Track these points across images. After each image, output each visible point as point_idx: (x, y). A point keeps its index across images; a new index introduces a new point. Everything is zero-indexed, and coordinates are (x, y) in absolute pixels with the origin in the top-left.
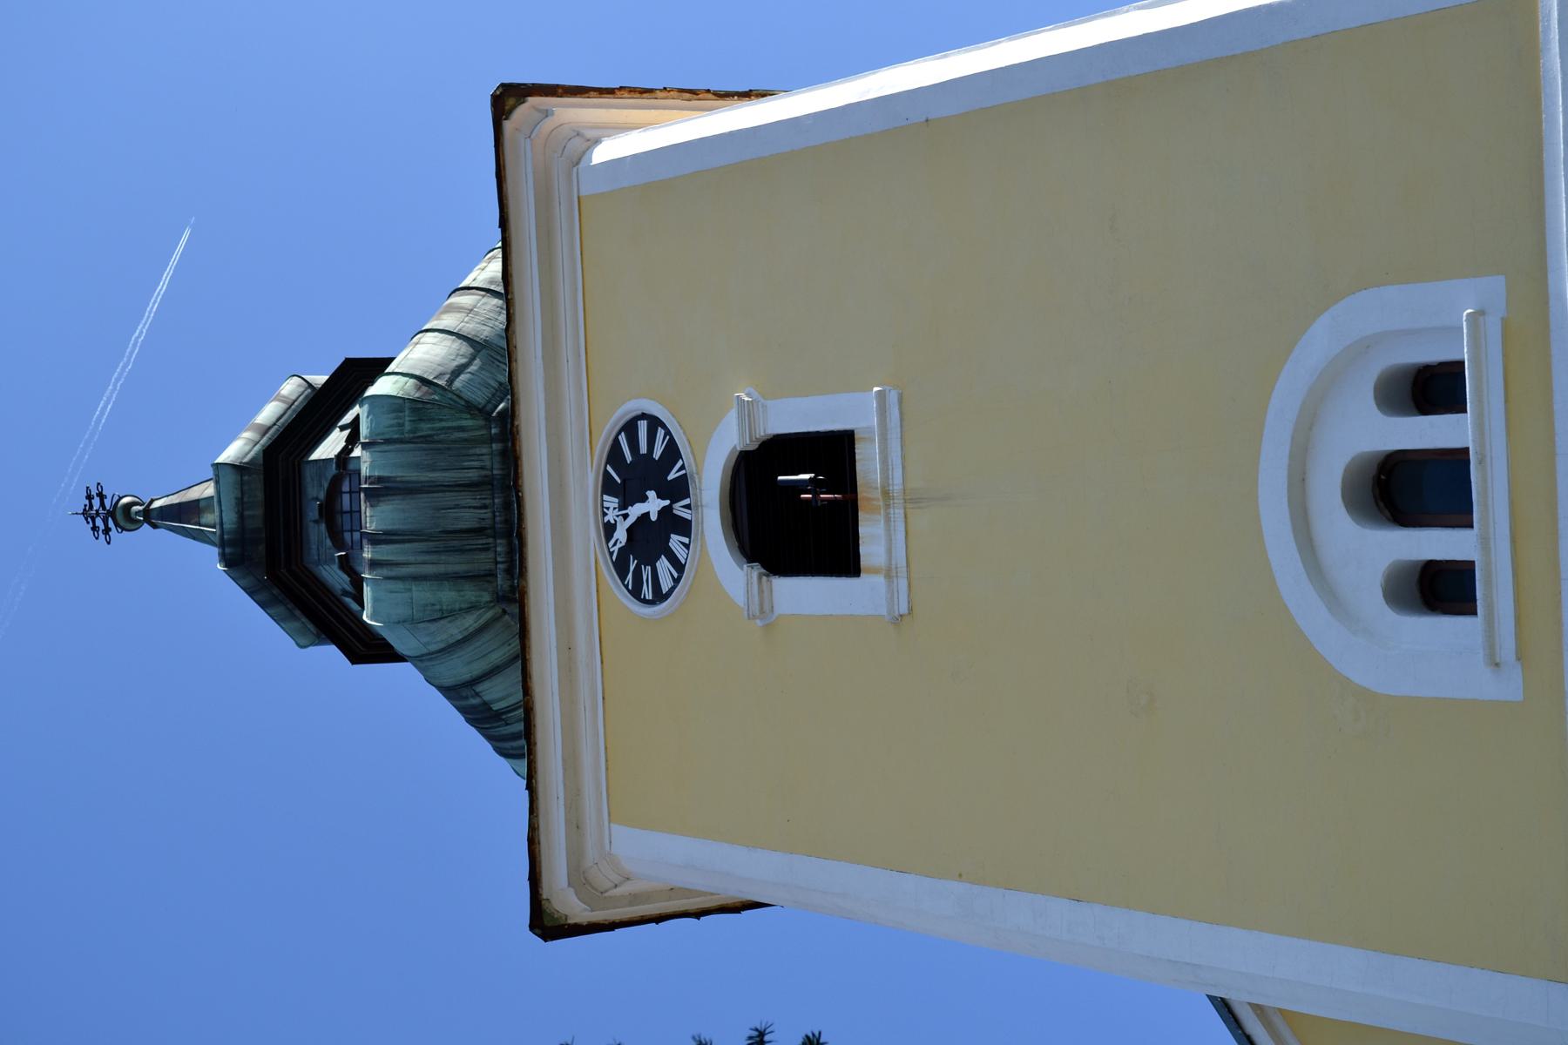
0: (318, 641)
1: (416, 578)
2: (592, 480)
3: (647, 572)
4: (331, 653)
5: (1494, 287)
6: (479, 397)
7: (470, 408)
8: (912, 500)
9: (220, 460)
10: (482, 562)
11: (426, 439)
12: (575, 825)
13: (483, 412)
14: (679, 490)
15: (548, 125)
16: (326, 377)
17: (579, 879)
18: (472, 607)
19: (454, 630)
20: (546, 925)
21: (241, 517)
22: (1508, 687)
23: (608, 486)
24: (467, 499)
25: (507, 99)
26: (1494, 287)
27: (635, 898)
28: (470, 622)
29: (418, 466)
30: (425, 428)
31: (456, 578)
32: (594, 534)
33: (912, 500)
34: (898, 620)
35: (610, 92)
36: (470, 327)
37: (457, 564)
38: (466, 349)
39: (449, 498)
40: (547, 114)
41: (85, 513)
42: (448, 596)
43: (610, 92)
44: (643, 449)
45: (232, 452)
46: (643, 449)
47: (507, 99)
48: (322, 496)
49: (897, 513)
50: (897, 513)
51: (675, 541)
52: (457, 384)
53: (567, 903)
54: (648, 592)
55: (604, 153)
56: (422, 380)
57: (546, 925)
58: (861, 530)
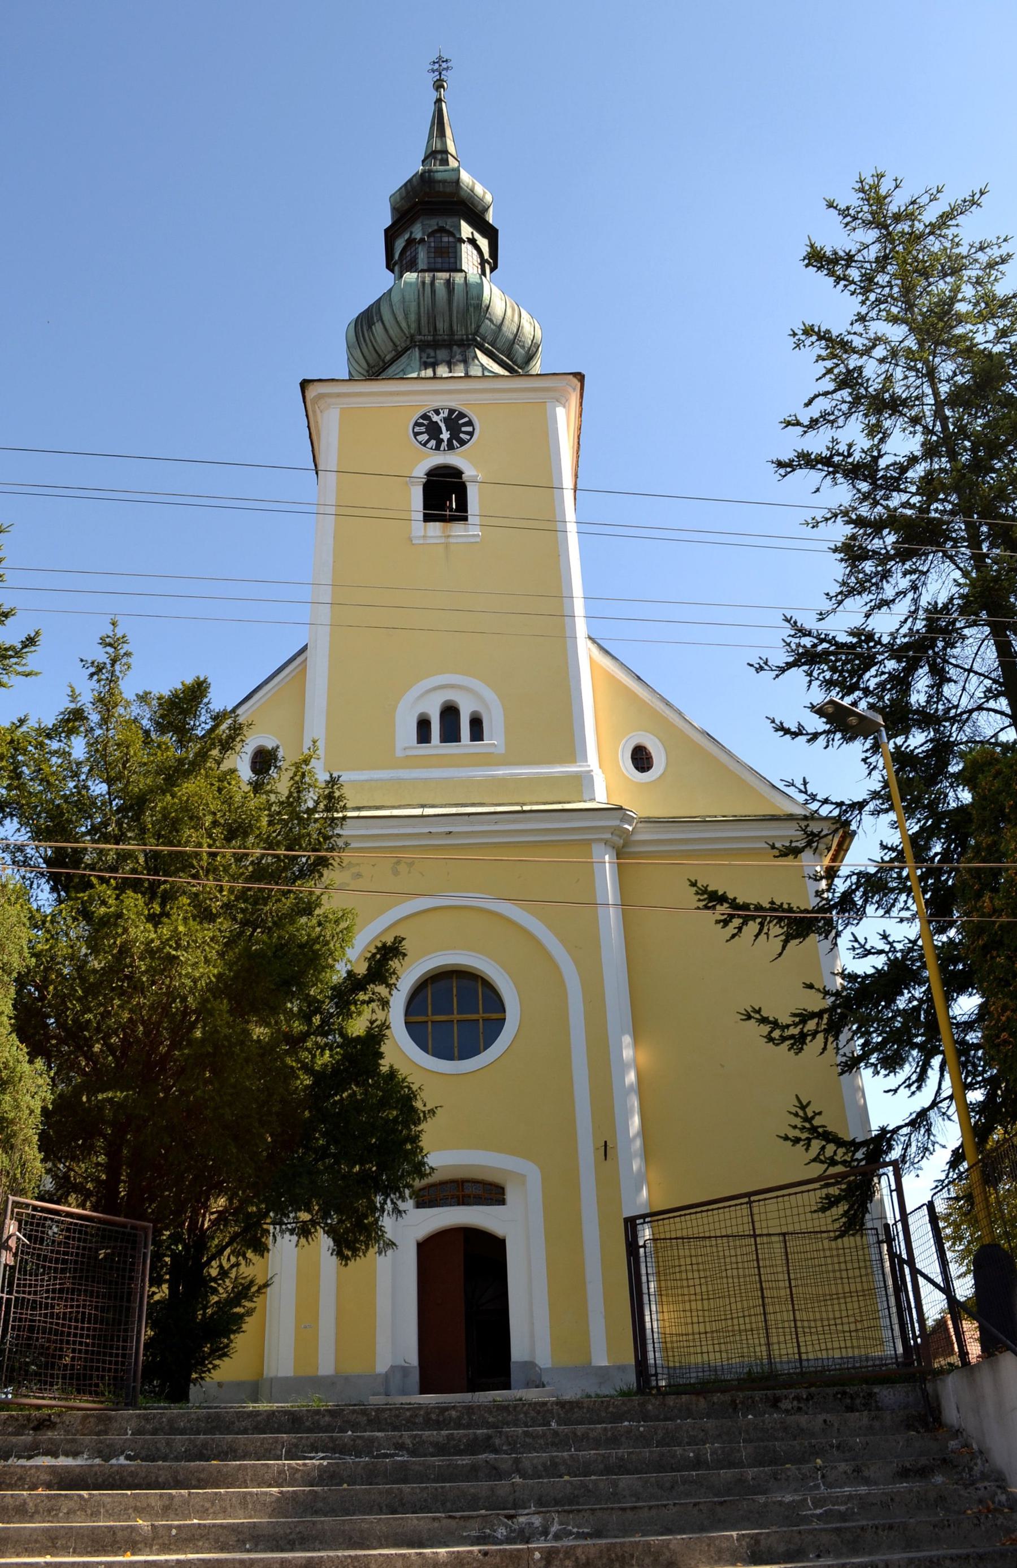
0: (394, 209)
1: (419, 304)
2: (453, 405)
3: (423, 429)
4: (388, 222)
5: (502, 750)
6: (482, 330)
7: (479, 327)
8: (447, 545)
9: (461, 170)
10: (425, 331)
11: (468, 309)
12: (339, 395)
13: (477, 332)
14: (451, 447)
15: (570, 390)
16: (491, 222)
17: (321, 396)
18: (409, 327)
19: (401, 317)
20: (304, 384)
21: (440, 181)
22: (399, 753)
23: (451, 411)
24: (447, 325)
25: (580, 377)
26: (502, 750)
27: (314, 412)
28: (404, 325)
29: (458, 306)
30: (472, 309)
31: (419, 321)
32: (436, 405)
33: (447, 545)
34: (410, 539)
35: (581, 404)
36: (507, 322)
37: (424, 321)
38: (499, 322)
39: (447, 318)
40: (574, 389)
41: (440, 58)
42: (413, 317)
43: (581, 404)
44: (464, 429)
45: (465, 177)
46: (464, 429)
47: (580, 377)
48: (448, 227)
49: (443, 540)
50: (443, 540)
51: (433, 443)
52: (487, 321)
53: (312, 392)
54: (417, 429)
55: (560, 412)
56: (488, 307)
57: (304, 384)
58: (437, 524)
